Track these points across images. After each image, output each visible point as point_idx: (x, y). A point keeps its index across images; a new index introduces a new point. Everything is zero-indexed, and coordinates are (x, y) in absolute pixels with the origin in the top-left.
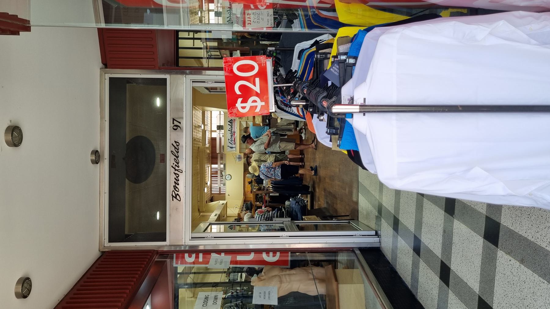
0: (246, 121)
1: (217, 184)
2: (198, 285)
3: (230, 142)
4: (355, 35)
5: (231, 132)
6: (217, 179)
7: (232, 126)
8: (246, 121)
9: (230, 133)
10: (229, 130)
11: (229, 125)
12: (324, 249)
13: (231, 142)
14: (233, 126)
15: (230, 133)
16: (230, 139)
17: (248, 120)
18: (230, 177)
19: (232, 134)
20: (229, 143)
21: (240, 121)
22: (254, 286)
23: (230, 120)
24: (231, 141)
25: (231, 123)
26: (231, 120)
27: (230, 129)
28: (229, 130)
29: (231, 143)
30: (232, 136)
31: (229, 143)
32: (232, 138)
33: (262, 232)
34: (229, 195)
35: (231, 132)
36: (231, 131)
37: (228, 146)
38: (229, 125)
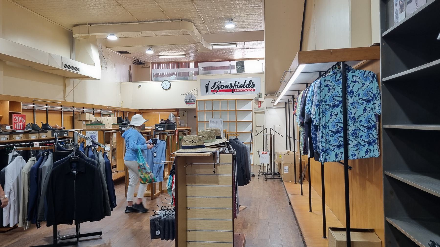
0: (252, 111)
1: (197, 80)
2: (256, 113)
3: (217, 84)
4: (153, 166)
5: (233, 85)
6: (165, 68)
7: (243, 86)
8: (252, 111)
9: (231, 84)
10: (236, 82)
11: (246, 81)
12: (5, 142)
13: (216, 87)
14: (243, 88)
15: (231, 84)
16: (221, 84)
17: (255, 113)
18: (168, 87)
19: (230, 88)
20: (215, 83)
21: (252, 100)
22: (374, 232)
23: (253, 83)
24: (218, 86)
25: (249, 85)
26: (254, 85)
27: (239, 83)
28: (236, 82)
29: (214, 85)
30: (227, 87)
31: (215, 83)
32: (222, 87)
33: (7, 97)
34: (139, 87)
35: (233, 85)
36: (235, 85)
37: (209, 81)
38: (246, 81)
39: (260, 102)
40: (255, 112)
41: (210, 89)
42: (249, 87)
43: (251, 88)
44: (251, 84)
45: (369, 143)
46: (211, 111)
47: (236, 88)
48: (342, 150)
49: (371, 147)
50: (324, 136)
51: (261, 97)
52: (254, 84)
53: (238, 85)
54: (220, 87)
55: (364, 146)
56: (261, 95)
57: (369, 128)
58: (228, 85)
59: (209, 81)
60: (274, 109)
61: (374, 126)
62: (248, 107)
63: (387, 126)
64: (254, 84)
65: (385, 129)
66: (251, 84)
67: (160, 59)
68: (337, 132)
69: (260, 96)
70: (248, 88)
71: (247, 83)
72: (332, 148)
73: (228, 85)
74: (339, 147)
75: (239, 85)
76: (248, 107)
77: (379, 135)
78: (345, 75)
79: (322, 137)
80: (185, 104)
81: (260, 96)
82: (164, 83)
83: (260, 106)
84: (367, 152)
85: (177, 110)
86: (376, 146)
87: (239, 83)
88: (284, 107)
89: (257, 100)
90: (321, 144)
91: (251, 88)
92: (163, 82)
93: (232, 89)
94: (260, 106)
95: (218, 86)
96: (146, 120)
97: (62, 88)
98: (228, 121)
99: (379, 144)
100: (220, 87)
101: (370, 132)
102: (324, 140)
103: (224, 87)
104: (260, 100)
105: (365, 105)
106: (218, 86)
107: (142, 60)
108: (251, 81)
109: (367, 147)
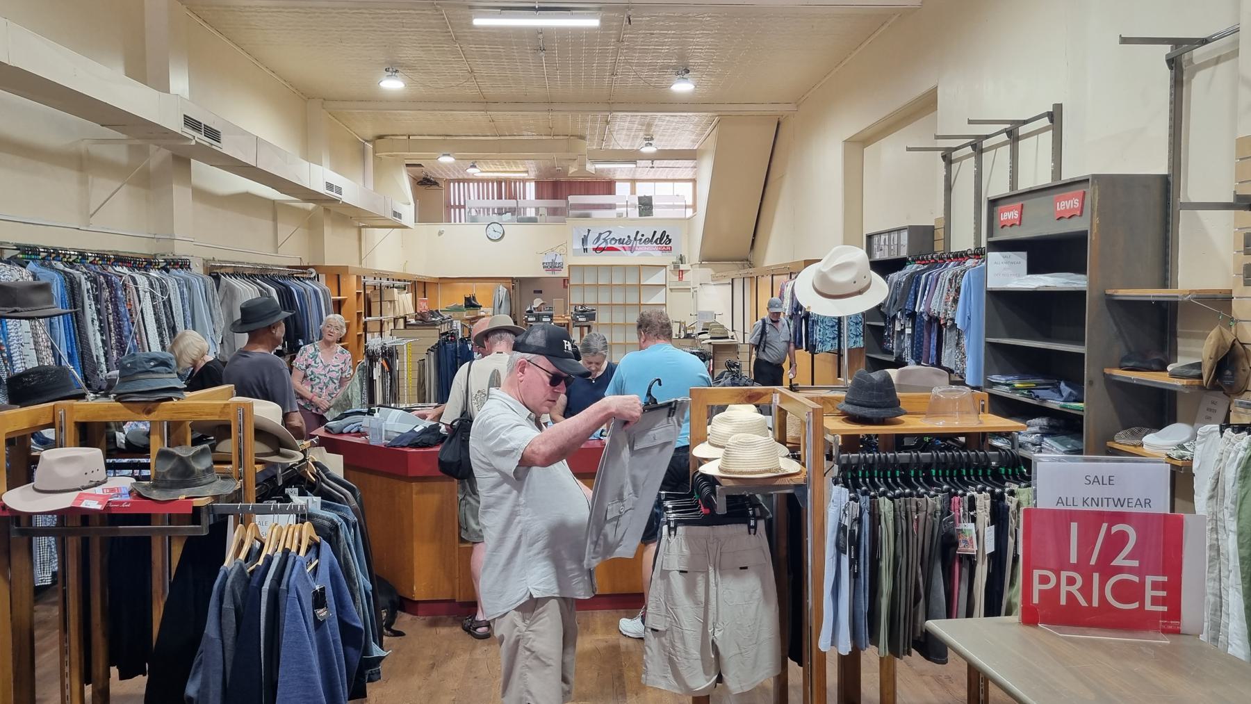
3: (603, 236)
8: (665, 285)
10: (638, 232)
11: (655, 232)
13: (601, 241)
16: (611, 237)
18: (497, 236)
20: (600, 234)
21: (665, 266)
23: (668, 236)
25: (661, 239)
26: (670, 240)
27: (643, 235)
28: (638, 232)
29: (598, 238)
31: (600, 234)
34: (440, 233)
37: (589, 230)
38: (655, 232)
39: (682, 271)
40: (671, 287)
41: (590, 246)
42: (660, 243)
43: (664, 245)
44: (665, 238)
45: (857, 336)
46: (609, 285)
47: (638, 245)
48: (836, 341)
49: (858, 339)
50: (822, 329)
51: (683, 262)
52: (670, 238)
53: (641, 240)
54: (609, 241)
55: (852, 338)
56: (683, 260)
57: (857, 324)
58: (624, 239)
59: (589, 230)
60: (714, 286)
61: (860, 322)
62: (657, 279)
63: (868, 323)
64: (670, 238)
65: (867, 325)
66: (665, 238)
67: (468, 174)
68: (832, 326)
69: (681, 259)
70: (660, 245)
71: (658, 236)
72: (828, 340)
73: (624, 239)
74: (834, 339)
75: (644, 238)
76: (657, 279)
77: (864, 329)
78: (914, 667)
79: (820, 331)
80: (544, 270)
81: (681, 259)
82: (491, 228)
83: (681, 279)
84: (854, 343)
85: (512, 278)
86: (862, 338)
87: (643, 235)
88: (729, 284)
89: (676, 266)
90: (817, 337)
91: (664, 245)
92: (489, 225)
93: (630, 245)
94: (681, 279)
95: (604, 239)
96: (542, 302)
97: (270, 223)
98: (625, 305)
99: (863, 336)
100: (609, 241)
101: (858, 326)
102: (821, 333)
103: (616, 242)
104: (682, 267)
105: (855, 339)
106: (604, 239)
107: (434, 174)
108: (665, 232)
109: (855, 339)
